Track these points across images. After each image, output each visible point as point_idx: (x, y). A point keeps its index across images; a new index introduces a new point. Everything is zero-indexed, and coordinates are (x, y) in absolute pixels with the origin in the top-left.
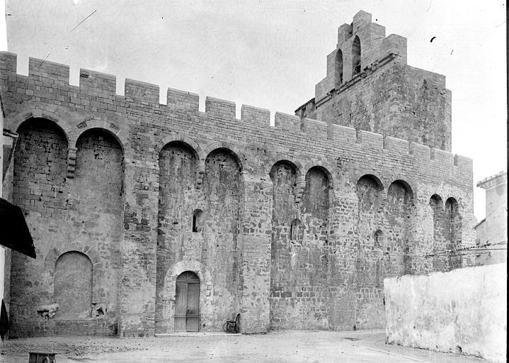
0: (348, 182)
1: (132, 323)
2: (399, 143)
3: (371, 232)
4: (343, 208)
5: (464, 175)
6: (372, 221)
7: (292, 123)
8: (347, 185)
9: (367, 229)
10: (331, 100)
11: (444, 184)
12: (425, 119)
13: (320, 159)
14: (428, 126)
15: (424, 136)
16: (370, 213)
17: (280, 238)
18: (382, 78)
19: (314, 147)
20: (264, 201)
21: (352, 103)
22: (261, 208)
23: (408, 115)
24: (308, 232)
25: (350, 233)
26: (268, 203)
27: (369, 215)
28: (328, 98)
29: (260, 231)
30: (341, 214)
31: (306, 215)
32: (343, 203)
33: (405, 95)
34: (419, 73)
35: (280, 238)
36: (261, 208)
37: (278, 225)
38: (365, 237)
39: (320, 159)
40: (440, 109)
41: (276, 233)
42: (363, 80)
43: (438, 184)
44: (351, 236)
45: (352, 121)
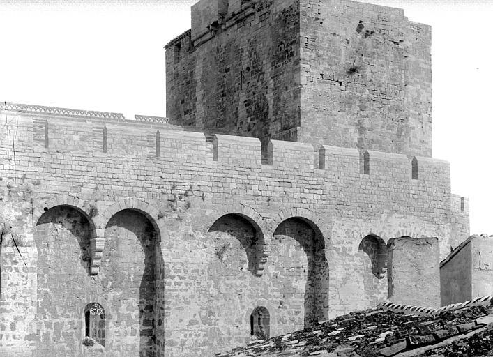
0: (190, 232)
1: (307, 271)
2: (294, 151)
3: (244, 312)
4: (177, 279)
5: (430, 194)
6: (246, 292)
7: (76, 138)
8: (187, 236)
9: (236, 308)
10: (215, 39)
11: (390, 215)
12: (363, 92)
13: (133, 196)
14: (368, 104)
15: (359, 123)
16: (242, 278)
17: (62, 339)
18: (283, 18)
19: (120, 176)
20: (21, 283)
21: (242, 52)
22: (14, 297)
23: (326, 87)
24: (117, 323)
25: (191, 323)
26: (28, 285)
27: (238, 282)
28: (209, 36)
29: (14, 337)
30: (176, 290)
31: (111, 295)
32: (177, 271)
33: (321, 53)
34: (197, 130)
35: (62, 339)
36: (14, 297)
37: (57, 317)
38: (231, 322)
39: (133, 196)
40: (393, 70)
41: (52, 331)
42: (258, 14)
43: (378, 213)
44: (194, 327)
45: (244, 86)
